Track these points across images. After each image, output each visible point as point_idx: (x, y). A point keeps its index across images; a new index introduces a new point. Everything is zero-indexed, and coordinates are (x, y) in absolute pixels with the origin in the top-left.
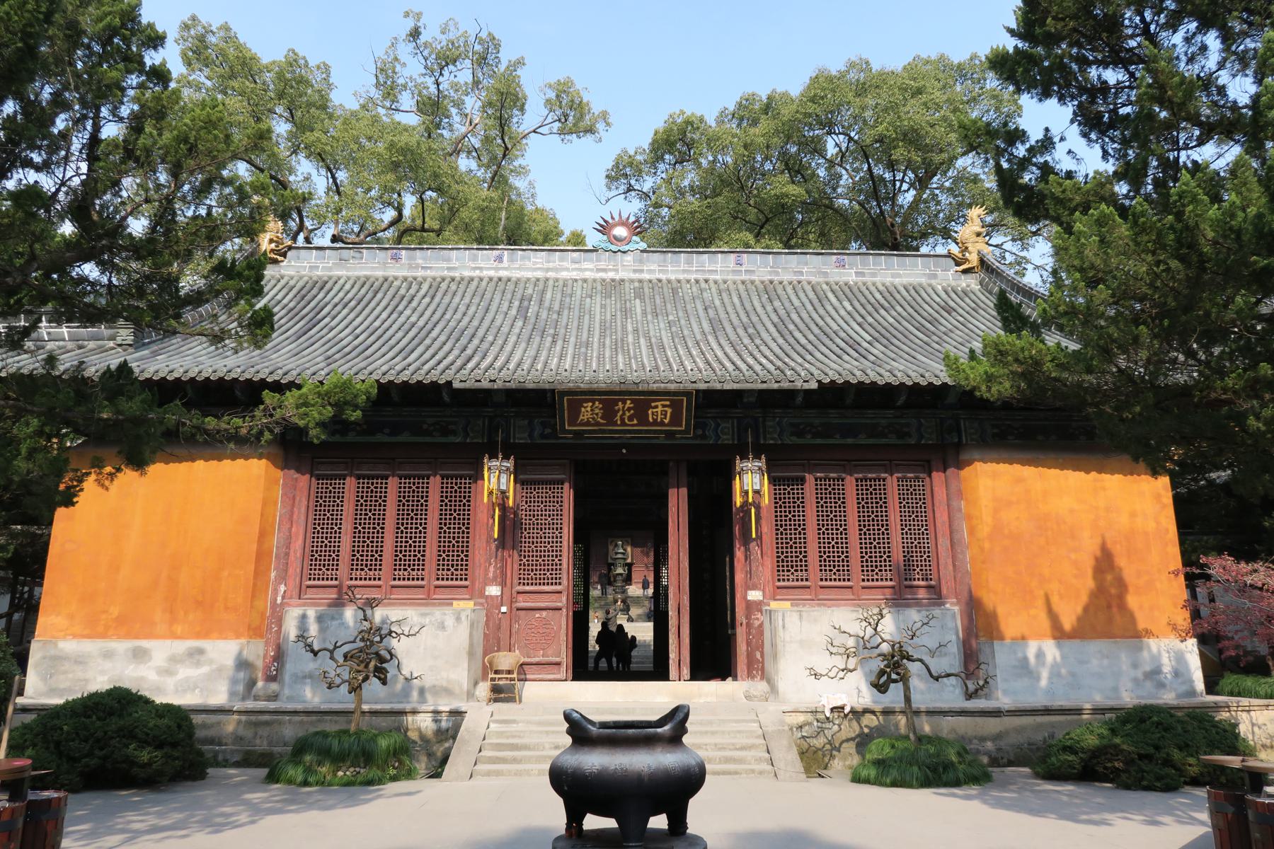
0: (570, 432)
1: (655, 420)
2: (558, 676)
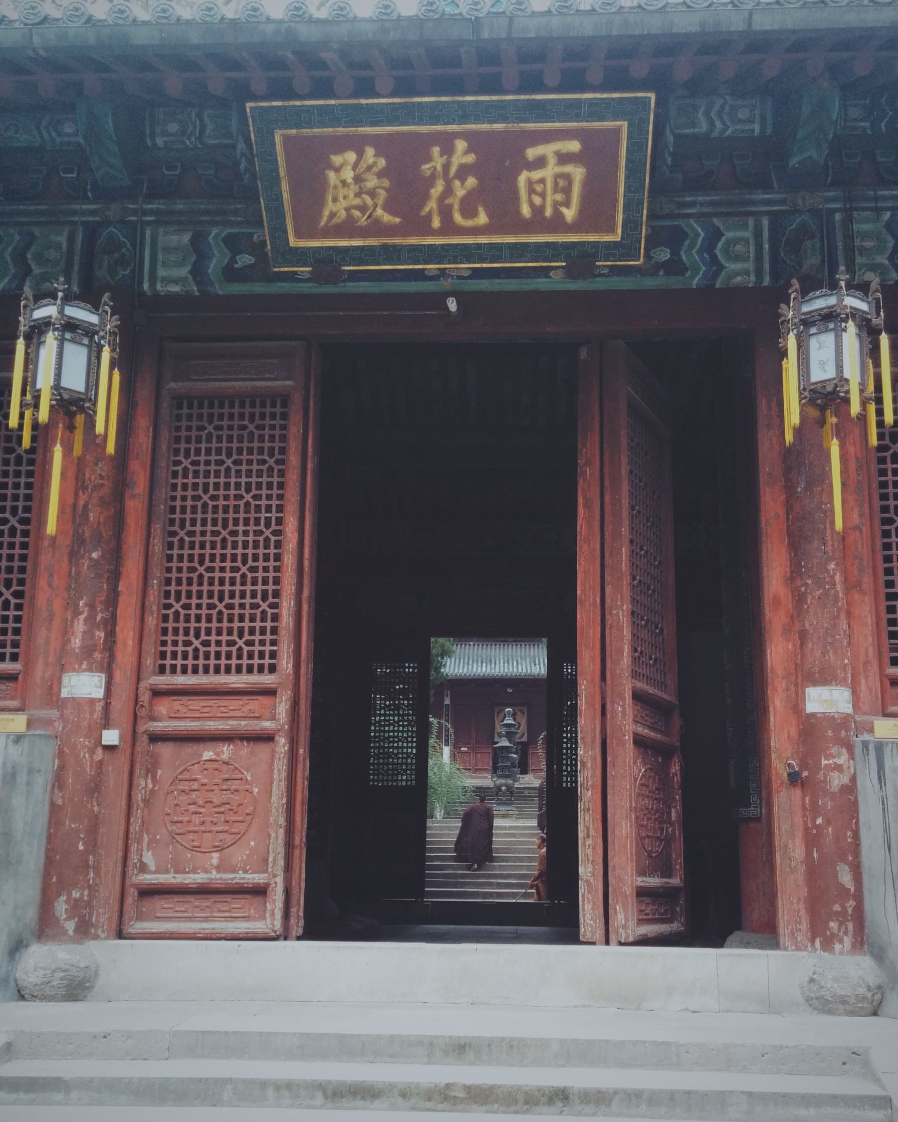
0: (301, 256)
1: (538, 211)
2: (259, 927)
